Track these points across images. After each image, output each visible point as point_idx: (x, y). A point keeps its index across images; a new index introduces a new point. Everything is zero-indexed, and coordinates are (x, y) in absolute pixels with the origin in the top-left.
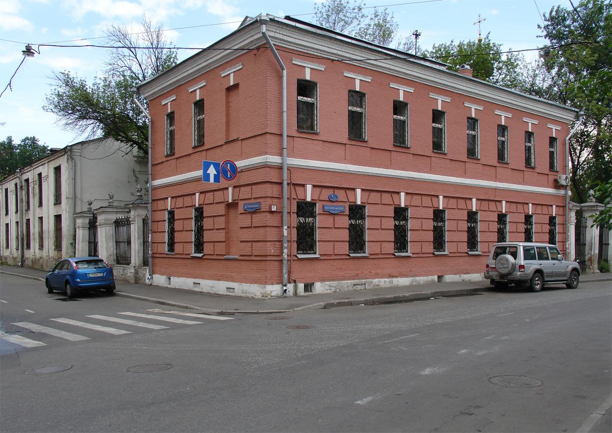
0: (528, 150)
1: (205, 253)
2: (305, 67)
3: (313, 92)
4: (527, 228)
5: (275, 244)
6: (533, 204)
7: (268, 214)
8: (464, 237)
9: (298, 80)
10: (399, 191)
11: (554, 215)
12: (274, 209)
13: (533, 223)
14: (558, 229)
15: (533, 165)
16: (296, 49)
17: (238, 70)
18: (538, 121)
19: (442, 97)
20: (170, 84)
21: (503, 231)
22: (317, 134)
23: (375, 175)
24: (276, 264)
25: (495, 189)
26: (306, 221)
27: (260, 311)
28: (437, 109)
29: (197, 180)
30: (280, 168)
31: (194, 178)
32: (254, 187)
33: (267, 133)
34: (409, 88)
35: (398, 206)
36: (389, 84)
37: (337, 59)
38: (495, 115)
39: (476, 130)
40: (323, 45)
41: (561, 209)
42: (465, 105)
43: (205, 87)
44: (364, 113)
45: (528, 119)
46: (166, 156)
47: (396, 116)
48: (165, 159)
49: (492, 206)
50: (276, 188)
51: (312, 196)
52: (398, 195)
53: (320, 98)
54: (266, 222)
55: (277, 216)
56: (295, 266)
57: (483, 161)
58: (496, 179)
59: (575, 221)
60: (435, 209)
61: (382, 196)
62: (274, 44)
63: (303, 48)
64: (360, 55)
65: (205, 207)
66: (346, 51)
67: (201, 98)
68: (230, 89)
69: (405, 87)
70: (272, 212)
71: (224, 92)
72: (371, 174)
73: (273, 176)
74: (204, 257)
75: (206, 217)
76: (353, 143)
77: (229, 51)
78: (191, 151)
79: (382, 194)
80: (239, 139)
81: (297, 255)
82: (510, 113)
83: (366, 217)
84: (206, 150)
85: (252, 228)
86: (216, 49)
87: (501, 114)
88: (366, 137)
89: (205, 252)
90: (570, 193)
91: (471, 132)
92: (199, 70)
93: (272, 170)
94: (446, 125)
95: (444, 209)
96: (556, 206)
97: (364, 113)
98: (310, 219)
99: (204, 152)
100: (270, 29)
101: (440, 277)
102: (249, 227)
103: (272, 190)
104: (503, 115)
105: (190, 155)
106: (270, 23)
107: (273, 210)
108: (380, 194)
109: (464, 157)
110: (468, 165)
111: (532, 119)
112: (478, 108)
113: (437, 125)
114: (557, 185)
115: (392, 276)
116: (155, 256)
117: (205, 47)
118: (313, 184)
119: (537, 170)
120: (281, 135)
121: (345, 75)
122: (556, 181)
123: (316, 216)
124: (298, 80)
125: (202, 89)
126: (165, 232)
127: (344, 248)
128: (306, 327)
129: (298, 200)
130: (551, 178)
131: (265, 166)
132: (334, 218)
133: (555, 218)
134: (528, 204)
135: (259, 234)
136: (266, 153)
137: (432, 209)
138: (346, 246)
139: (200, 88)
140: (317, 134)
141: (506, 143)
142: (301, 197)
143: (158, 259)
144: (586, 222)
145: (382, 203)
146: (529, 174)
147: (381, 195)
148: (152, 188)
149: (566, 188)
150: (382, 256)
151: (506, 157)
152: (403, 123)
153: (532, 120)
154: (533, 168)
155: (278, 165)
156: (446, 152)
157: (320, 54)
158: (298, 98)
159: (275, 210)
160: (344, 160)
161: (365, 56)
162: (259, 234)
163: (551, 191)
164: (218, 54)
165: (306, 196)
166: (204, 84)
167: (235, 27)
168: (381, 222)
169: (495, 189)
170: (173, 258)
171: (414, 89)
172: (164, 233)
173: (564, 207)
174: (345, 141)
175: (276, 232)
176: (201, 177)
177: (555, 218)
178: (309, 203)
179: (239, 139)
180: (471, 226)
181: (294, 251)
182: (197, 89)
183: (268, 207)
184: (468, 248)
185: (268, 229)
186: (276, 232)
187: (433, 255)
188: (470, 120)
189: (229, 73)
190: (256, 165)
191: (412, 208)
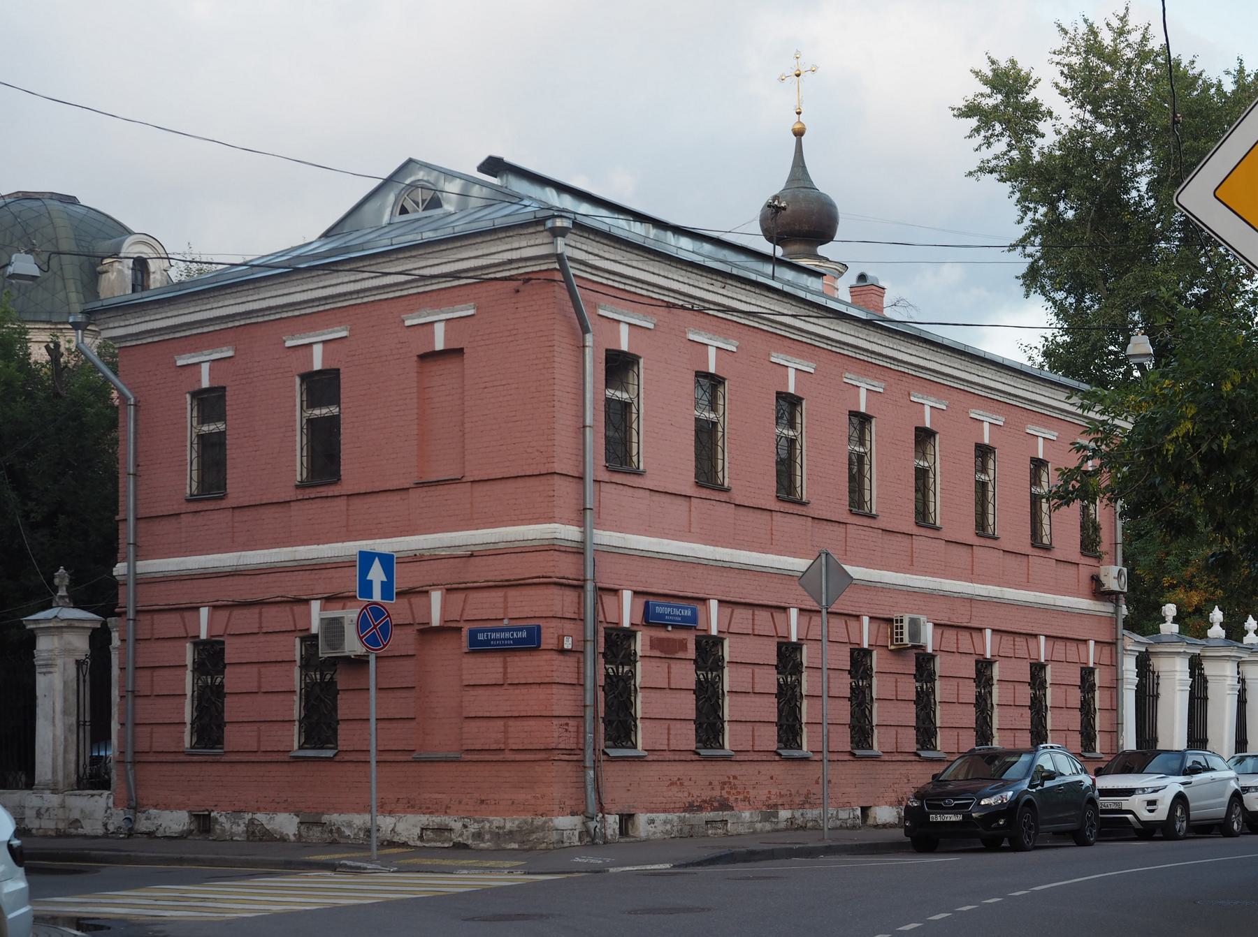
0: (982, 487)
2: (619, 321)
3: (627, 377)
4: (857, 686)
5: (567, 724)
6: (1046, 636)
7: (555, 656)
8: (687, 705)
9: (607, 350)
10: (787, 605)
11: (1091, 665)
12: (568, 644)
13: (1048, 685)
14: (1099, 699)
15: (1046, 541)
16: (605, 281)
18: (1056, 434)
19: (869, 381)
21: (794, 692)
22: (638, 473)
23: (745, 567)
24: (569, 768)
25: (971, 600)
26: (618, 673)
28: (706, 371)
30: (579, 550)
33: (555, 473)
34: (806, 363)
35: (857, 647)
36: (769, 355)
37: (681, 303)
38: (970, 422)
39: (868, 443)
40: (656, 271)
41: (1106, 650)
42: (912, 399)
44: (721, 422)
45: (1037, 428)
46: (188, 501)
47: (612, 391)
49: (965, 640)
50: (570, 596)
51: (631, 617)
52: (1035, 640)
53: (645, 392)
55: (571, 661)
56: (610, 771)
57: (947, 534)
58: (972, 576)
59: (1136, 680)
60: (1034, 661)
61: (756, 617)
62: (574, 275)
63: (783, 328)
64: (753, 301)
66: (696, 284)
69: (798, 361)
70: (562, 651)
72: (680, 559)
73: (565, 567)
76: (618, 478)
77: (413, 277)
78: (291, 494)
79: (756, 612)
80: (464, 480)
81: (607, 751)
82: (999, 414)
83: (725, 664)
87: (981, 418)
88: (727, 480)
90: (1124, 610)
91: (785, 432)
93: (563, 556)
94: (938, 459)
95: (870, 648)
96: (1096, 642)
97: (721, 422)
98: (626, 668)
99: (342, 502)
100: (573, 244)
101: (865, 810)
103: (564, 602)
104: (794, 364)
106: (572, 231)
107: (566, 647)
108: (750, 612)
109: (909, 525)
110: (917, 542)
111: (1046, 427)
112: (938, 406)
113: (618, 394)
114: (1099, 591)
115: (146, 834)
118: (635, 589)
119: (1058, 553)
120: (581, 478)
121: (691, 337)
122: (1095, 579)
123: (636, 661)
124: (607, 350)
128: (709, 910)
129: (605, 625)
130: (1085, 572)
131: (551, 547)
132: (669, 667)
133: (868, 653)
134: (1036, 636)
135: (531, 701)
136: (551, 520)
137: (847, 649)
138: (689, 732)
140: (638, 473)
141: (990, 488)
142: (612, 618)
144: (1158, 684)
145: (756, 633)
146: (924, 543)
147: (753, 615)
148: (136, 579)
149: (1117, 599)
150: (755, 757)
151: (991, 522)
152: (626, 406)
153: (1046, 431)
154: (1048, 548)
155: (574, 545)
156: (641, 467)
157: (648, 290)
158: (607, 393)
159: (570, 647)
160: (684, 534)
161: (772, 308)
162: (531, 701)
163: (1085, 604)
165: (620, 616)
168: (753, 678)
169: (971, 600)
171: (814, 366)
173: (1113, 644)
174: (690, 490)
175: (570, 698)
176: (353, 558)
177: (868, 653)
178: (625, 629)
179: (464, 480)
180: (922, 688)
181: (602, 744)
183: (555, 641)
184: (779, 741)
185: (555, 689)
186: (570, 698)
187: (851, 758)
188: (855, 420)
190: (517, 544)
191: (734, 639)
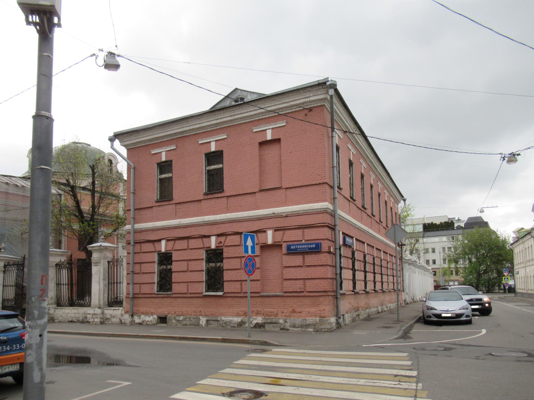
1: (225, 291)
17: (279, 127)
20: (166, 136)
27: (493, 354)
29: (324, 211)
31: (250, 218)
32: (306, 230)
43: (226, 140)
48: (155, 204)
54: (326, 261)
65: (225, 250)
67: (218, 149)
68: (264, 144)
71: (257, 145)
73: (328, 220)
74: (224, 295)
75: (225, 258)
78: (201, 197)
84: (227, 197)
85: (304, 267)
86: (253, 106)
89: (226, 290)
92: (217, 124)
102: (299, 266)
103: (326, 233)
105: (200, 200)
116: (137, 296)
117: (268, 91)
125: (218, 142)
126: (155, 273)
127: (202, 288)
139: (216, 141)
143: (141, 300)
164: (254, 110)
166: (225, 137)
167: (207, 108)
170: (237, 297)
172: (154, 274)
182: (269, 129)
189: (211, 140)
